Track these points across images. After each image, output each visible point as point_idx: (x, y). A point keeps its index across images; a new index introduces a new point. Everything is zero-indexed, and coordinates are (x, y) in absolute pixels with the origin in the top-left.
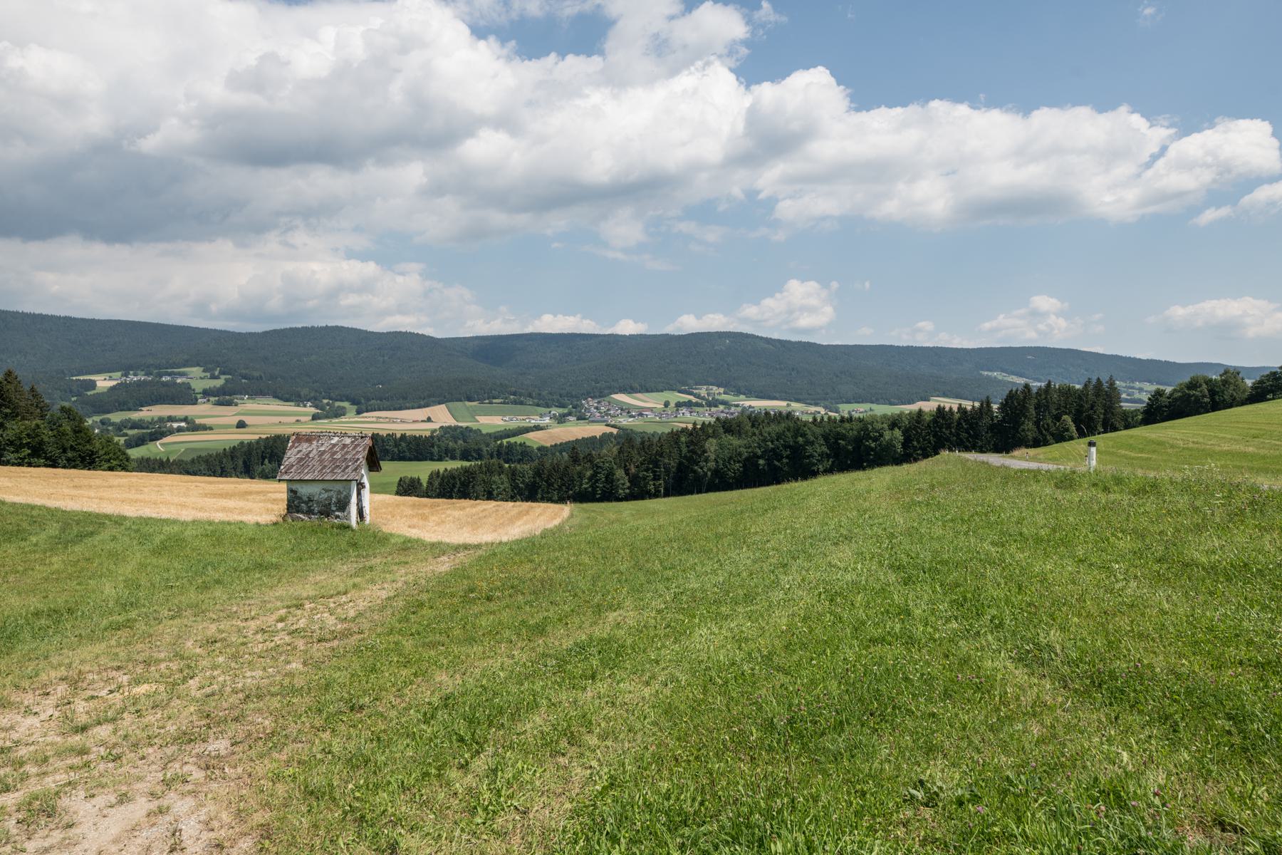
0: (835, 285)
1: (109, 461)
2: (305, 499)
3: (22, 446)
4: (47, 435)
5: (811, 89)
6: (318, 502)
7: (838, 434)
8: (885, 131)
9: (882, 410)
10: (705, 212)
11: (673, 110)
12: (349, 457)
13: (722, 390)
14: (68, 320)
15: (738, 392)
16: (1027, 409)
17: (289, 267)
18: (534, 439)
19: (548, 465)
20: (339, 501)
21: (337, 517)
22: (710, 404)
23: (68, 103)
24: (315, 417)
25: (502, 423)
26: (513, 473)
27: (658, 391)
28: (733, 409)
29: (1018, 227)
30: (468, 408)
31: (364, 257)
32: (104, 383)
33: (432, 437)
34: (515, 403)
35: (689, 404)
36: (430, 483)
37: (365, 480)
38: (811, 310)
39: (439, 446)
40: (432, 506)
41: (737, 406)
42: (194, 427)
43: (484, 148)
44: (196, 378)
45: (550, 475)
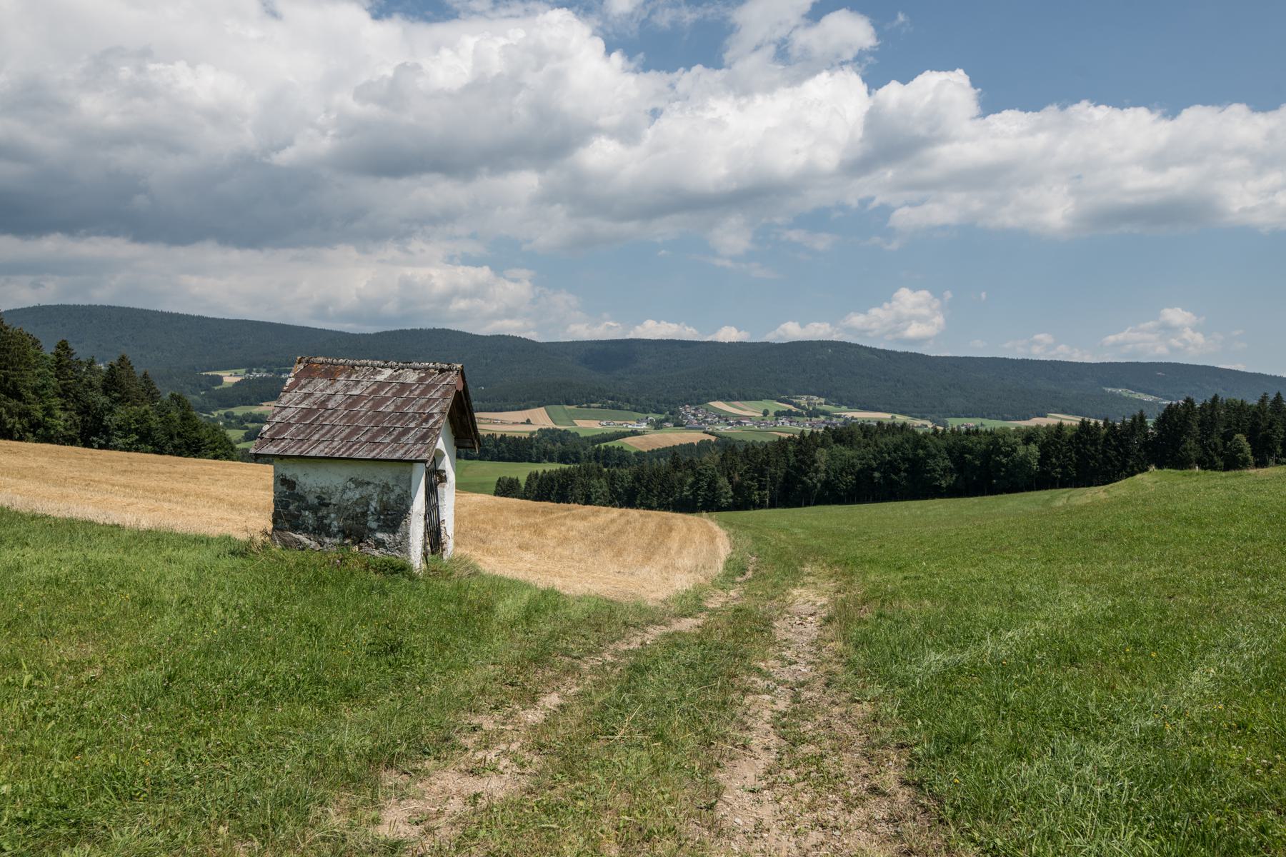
0: (948, 295)
1: (214, 449)
2: (312, 499)
3: (130, 431)
4: (155, 421)
5: (942, 91)
6: (339, 509)
7: (964, 447)
8: (1012, 133)
9: (1012, 425)
10: (817, 220)
11: (793, 118)
12: (410, 410)
13: (823, 400)
14: (201, 319)
15: (840, 403)
16: (1190, 426)
17: (409, 271)
19: (647, 470)
20: (385, 508)
21: (380, 544)
23: (218, 116)
26: (612, 479)
27: (757, 399)
28: (835, 420)
29: (1158, 236)
30: (565, 412)
31: (468, 261)
32: (229, 378)
34: (613, 407)
35: (788, 414)
36: (528, 484)
37: (447, 465)
38: (921, 320)
40: (544, 513)
41: (839, 417)
43: (601, 155)
45: (650, 481)
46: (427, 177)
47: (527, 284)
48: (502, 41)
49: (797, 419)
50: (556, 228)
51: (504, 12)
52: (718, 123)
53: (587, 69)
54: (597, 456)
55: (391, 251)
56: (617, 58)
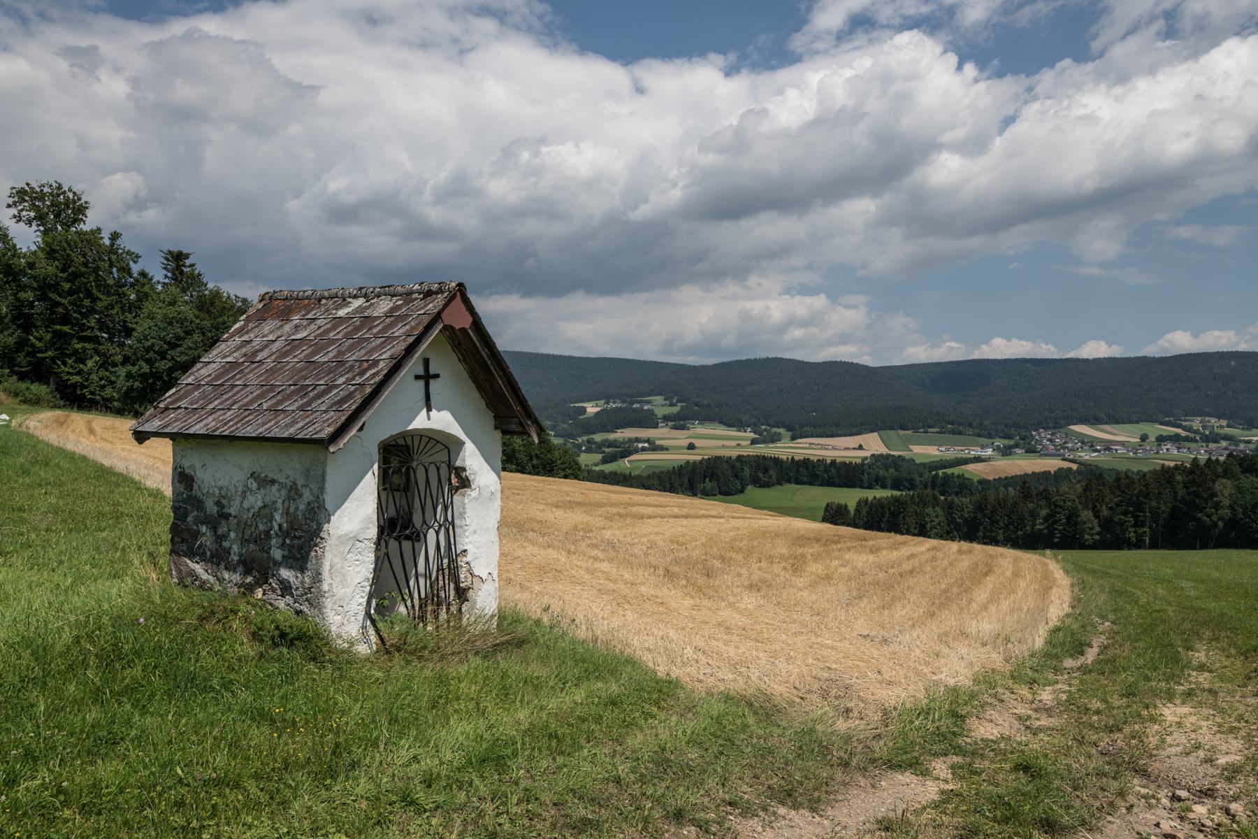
10: (1218, 211)
13: (1224, 423)
17: (748, 305)
18: (974, 471)
19: (992, 498)
21: (286, 589)
22: (1206, 439)
24: (754, 442)
25: (937, 453)
26: (950, 507)
27: (1131, 422)
28: (1242, 446)
31: (806, 291)
33: (863, 464)
34: (953, 432)
35: (1176, 439)
36: (857, 510)
39: (869, 474)
41: (1249, 442)
42: (655, 448)
43: (946, 170)
44: (659, 405)
46: (764, 216)
47: (864, 309)
48: (848, 73)
49: (1188, 444)
50: (896, 250)
51: (847, 46)
52: (1090, 119)
53: (931, 79)
54: (934, 483)
55: (732, 288)
56: (970, 70)
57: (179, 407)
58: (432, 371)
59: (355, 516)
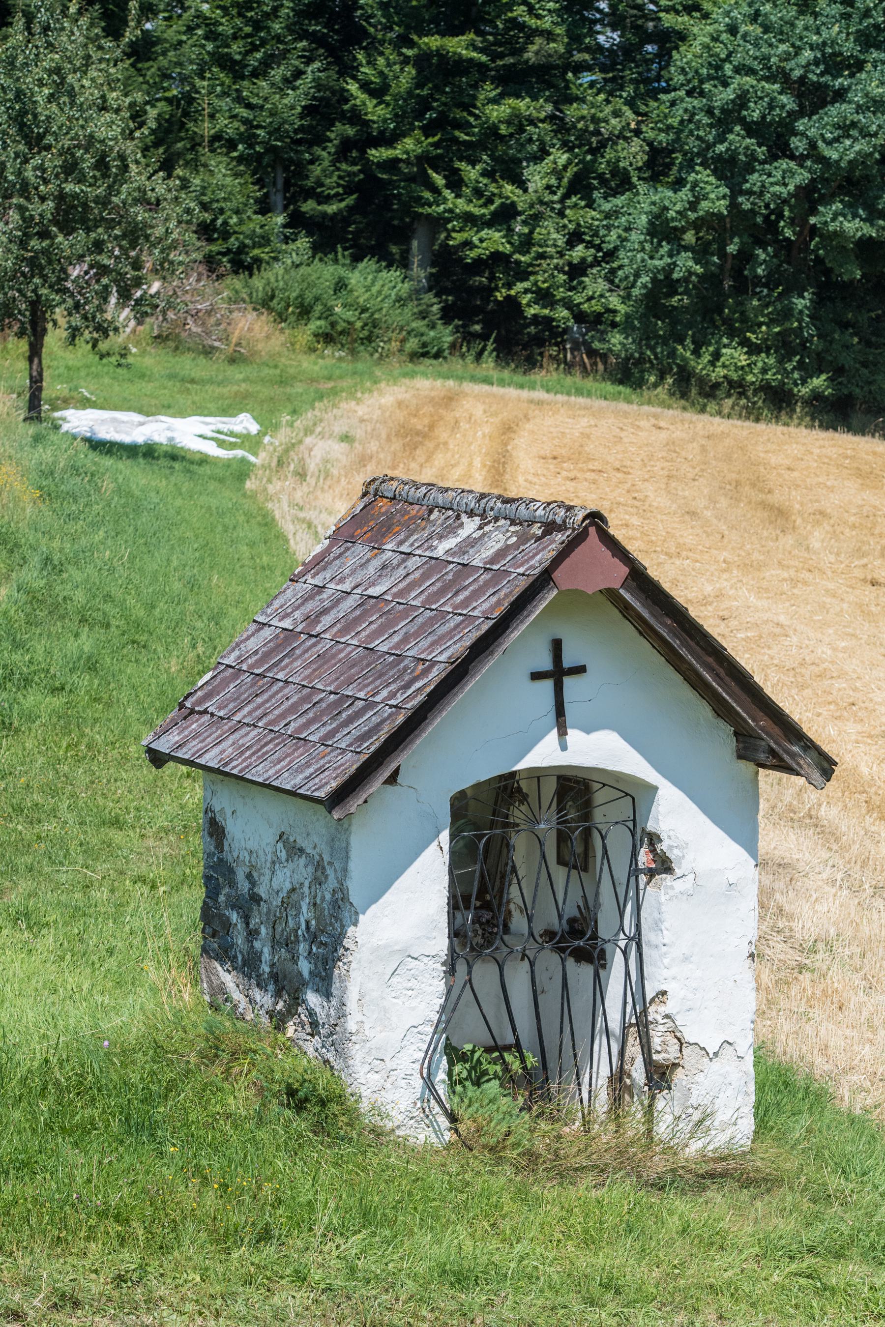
57: (205, 712)
58: (567, 663)
59: (403, 920)
